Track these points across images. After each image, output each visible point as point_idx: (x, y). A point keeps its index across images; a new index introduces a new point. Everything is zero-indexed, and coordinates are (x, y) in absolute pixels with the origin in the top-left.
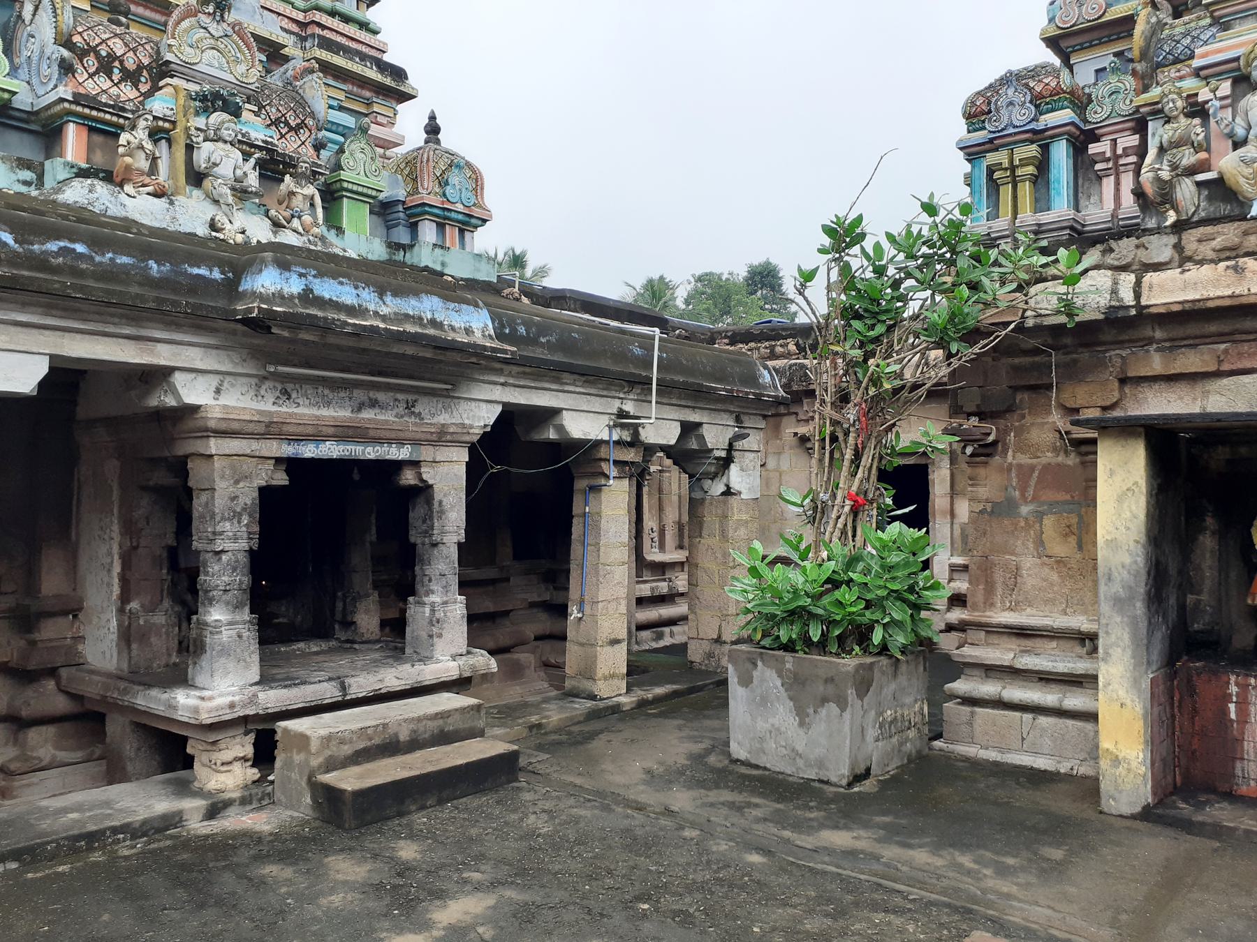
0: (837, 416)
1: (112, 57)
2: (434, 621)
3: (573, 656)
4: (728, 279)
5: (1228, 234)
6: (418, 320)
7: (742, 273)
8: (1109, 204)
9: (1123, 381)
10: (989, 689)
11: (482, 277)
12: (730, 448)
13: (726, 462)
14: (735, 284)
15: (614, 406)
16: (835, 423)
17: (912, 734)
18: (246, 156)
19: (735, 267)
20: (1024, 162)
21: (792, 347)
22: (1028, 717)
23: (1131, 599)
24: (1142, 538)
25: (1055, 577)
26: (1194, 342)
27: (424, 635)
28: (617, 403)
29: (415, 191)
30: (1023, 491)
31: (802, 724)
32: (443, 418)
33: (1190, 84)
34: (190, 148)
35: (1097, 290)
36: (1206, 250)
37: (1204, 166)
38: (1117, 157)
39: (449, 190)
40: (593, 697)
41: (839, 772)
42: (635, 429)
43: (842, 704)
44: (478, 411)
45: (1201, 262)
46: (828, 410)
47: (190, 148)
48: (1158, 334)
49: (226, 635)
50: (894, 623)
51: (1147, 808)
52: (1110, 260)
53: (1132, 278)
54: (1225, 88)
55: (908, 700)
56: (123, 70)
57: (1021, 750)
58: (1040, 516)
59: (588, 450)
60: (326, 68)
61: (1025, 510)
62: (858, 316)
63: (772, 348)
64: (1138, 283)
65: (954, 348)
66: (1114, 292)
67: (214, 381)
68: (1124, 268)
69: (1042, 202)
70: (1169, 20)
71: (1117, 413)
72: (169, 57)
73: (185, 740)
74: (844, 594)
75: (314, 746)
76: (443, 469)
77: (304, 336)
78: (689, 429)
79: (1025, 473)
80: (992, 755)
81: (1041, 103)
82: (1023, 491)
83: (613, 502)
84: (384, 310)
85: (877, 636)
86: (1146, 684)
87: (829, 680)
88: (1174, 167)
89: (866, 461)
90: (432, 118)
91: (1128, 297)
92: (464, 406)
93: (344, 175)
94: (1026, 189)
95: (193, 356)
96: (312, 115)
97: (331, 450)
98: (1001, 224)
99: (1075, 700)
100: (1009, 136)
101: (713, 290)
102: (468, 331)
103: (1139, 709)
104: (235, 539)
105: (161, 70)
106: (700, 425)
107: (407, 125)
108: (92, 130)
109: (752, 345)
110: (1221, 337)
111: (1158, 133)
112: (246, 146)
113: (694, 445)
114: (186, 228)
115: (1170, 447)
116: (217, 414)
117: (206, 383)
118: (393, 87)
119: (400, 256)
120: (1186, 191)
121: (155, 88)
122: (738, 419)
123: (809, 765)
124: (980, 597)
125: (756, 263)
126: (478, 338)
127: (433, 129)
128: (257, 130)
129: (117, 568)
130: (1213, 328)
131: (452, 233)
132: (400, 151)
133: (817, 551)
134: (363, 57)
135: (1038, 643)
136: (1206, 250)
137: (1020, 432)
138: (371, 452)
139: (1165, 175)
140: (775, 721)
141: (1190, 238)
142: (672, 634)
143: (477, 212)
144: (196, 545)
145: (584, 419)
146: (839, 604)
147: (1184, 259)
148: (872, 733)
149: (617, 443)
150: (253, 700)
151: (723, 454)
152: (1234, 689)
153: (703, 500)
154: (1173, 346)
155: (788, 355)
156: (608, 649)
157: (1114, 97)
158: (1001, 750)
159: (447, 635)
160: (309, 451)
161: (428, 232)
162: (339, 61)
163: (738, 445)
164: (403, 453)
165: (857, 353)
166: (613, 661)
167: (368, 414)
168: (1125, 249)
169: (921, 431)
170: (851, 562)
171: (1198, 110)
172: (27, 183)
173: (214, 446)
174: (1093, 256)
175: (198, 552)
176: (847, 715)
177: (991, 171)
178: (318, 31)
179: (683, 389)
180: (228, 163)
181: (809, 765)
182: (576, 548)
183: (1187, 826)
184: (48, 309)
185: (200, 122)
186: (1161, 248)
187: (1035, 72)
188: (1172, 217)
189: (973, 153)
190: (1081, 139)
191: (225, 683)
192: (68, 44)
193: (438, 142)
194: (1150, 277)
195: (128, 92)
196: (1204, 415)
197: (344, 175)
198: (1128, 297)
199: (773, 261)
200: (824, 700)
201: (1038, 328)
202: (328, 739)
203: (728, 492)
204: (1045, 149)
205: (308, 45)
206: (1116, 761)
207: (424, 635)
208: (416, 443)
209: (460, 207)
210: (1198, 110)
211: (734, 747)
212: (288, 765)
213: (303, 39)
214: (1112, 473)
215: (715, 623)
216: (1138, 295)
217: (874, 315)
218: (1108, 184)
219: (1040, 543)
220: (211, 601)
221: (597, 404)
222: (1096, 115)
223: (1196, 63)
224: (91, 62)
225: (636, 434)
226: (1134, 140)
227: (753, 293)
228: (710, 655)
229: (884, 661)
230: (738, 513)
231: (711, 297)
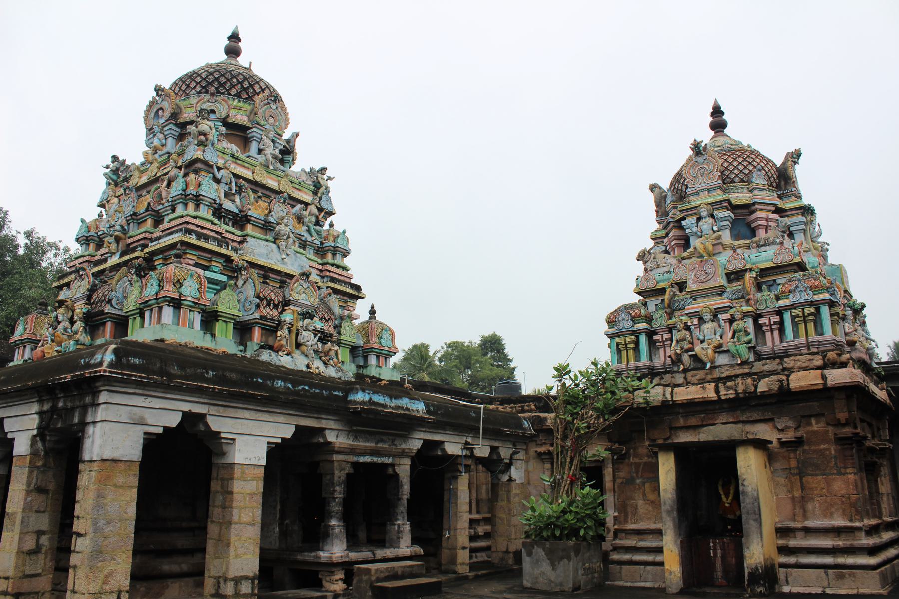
0: (563, 444)
1: (271, 300)
2: (399, 531)
3: (445, 554)
4: (468, 346)
5: (700, 374)
6: (401, 408)
7: (477, 341)
8: (662, 359)
9: (671, 429)
10: (627, 557)
11: (394, 379)
12: (511, 459)
13: (509, 466)
14: (474, 349)
15: (464, 440)
16: (562, 447)
17: (596, 575)
18: (315, 335)
19: (472, 337)
20: (630, 343)
21: (533, 407)
22: (642, 567)
23: (672, 510)
24: (674, 487)
25: (651, 508)
26: (694, 414)
27: (395, 537)
28: (465, 438)
29: (367, 342)
30: (637, 473)
31: (553, 569)
32: (403, 446)
33: (685, 318)
34: (297, 335)
35: (657, 394)
36: (694, 380)
37: (692, 350)
38: (664, 342)
39: (382, 341)
40: (455, 572)
41: (569, 586)
42: (472, 450)
43: (569, 559)
44: (415, 444)
45: (693, 384)
46: (559, 441)
47: (297, 335)
48: (681, 411)
49: (337, 530)
50: (589, 527)
51: (681, 589)
52: (662, 382)
53: (670, 389)
54: (696, 321)
55: (595, 560)
56: (274, 304)
57: (641, 581)
58: (644, 483)
59: (453, 460)
60: (336, 291)
61: (638, 481)
62: (569, 404)
63: (523, 407)
64: (672, 392)
65: (607, 417)
66: (664, 395)
67: (335, 433)
68: (668, 385)
69: (637, 358)
70: (678, 292)
71: (670, 441)
72: (291, 298)
73: (317, 572)
74: (569, 517)
75: (373, 572)
76: (402, 467)
77: (371, 416)
78: (494, 449)
79: (637, 465)
80: (629, 584)
81: (634, 320)
82: (637, 473)
83: (463, 484)
84: (392, 405)
85: (582, 532)
86: (679, 542)
87: (564, 550)
88: (682, 349)
89: (575, 462)
90: (372, 307)
91: (669, 397)
92: (410, 441)
93: (342, 337)
94: (631, 353)
95: (331, 424)
96: (333, 314)
97: (368, 459)
98: (623, 366)
99: (658, 558)
100: (626, 330)
101: (460, 354)
102: (418, 411)
103: (677, 552)
104: (340, 493)
105: (286, 303)
106: (498, 447)
107: (361, 310)
108: (263, 329)
109: (512, 405)
110: (701, 412)
111: (676, 335)
112: (315, 332)
113: (495, 457)
114: (300, 369)
115: (683, 454)
116: (337, 445)
117: (336, 436)
118: (355, 293)
119: (361, 371)
120: (685, 358)
121: (284, 310)
122: (514, 445)
123: (556, 585)
124: (622, 519)
125: (486, 335)
126: (421, 414)
127: (372, 312)
128: (319, 325)
129: (278, 507)
130: (698, 409)
131: (382, 359)
132: (356, 323)
133: (557, 500)
134: (345, 283)
135: (646, 536)
136: (694, 380)
137: (635, 449)
138: (379, 460)
139: (678, 352)
140: (542, 569)
141: (689, 374)
142: (477, 557)
143: (393, 350)
144: (323, 495)
145: (453, 447)
146: (567, 520)
147: (687, 383)
148: (581, 572)
149: (466, 456)
150: (347, 556)
151: (508, 461)
152: (712, 544)
153: (498, 484)
154: (686, 416)
155: (531, 411)
156: (461, 551)
157: (661, 320)
158: (632, 582)
159: (404, 538)
160: (362, 459)
161: (372, 360)
162: (337, 286)
163: (515, 457)
164: (389, 460)
165: (570, 419)
166: (463, 556)
167: (380, 445)
168: (667, 378)
169: (597, 450)
170: (571, 503)
171: (688, 328)
172: (241, 351)
173: (335, 457)
174: (656, 380)
175: (325, 498)
176: (571, 563)
177: (618, 345)
178: (328, 273)
179: (492, 433)
180: (308, 338)
181: (556, 585)
182: (446, 505)
183: (695, 594)
184: (298, 409)
185: (300, 324)
186: (679, 379)
187: (631, 307)
188: (682, 368)
189: (611, 337)
190: (650, 334)
191: (336, 550)
192: (258, 297)
193: (375, 318)
194: (676, 390)
195: (275, 313)
196: (699, 442)
197: (342, 337)
198: (669, 397)
199: (498, 334)
200: (562, 558)
201: (638, 408)
202: (377, 570)
203: (511, 480)
204: (637, 337)
205: (325, 280)
206: (671, 573)
207: (395, 537)
208: (394, 456)
209: (386, 348)
210: (688, 328)
211: (525, 582)
212: (360, 581)
213: (323, 277)
214: (663, 464)
215: (505, 543)
216: (672, 397)
217: (576, 403)
218: (662, 351)
219: (644, 495)
220: (331, 517)
221: (457, 439)
222: (656, 325)
223: (686, 312)
224: (265, 303)
225: (472, 452)
226: (668, 336)
227: (485, 355)
228: (502, 559)
229: (585, 543)
230: (515, 491)
231: (458, 357)
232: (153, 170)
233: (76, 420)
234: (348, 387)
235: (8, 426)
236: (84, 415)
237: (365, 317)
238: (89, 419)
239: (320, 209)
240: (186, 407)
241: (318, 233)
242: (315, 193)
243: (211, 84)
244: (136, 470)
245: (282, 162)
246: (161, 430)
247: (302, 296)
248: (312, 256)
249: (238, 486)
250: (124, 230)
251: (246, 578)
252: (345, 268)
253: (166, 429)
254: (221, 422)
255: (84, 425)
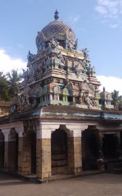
97: (108, 133)
107: (100, 89)
127: (104, 89)
132: (100, 92)
160: (106, 133)
164: (114, 133)
173: (100, 133)
232: (41, 56)
233: (34, 128)
234: (101, 113)
235: (3, 131)
236: (36, 128)
237: (102, 91)
238: (37, 129)
239: (87, 61)
240: (60, 124)
241: (87, 68)
242: (85, 56)
243: (52, 29)
244: (50, 140)
245: (75, 49)
246: (55, 130)
247: (85, 87)
248: (85, 75)
249: (75, 143)
250: (35, 74)
251: (79, 168)
252: (95, 77)
253: (56, 130)
254: (70, 126)
255: (36, 130)
